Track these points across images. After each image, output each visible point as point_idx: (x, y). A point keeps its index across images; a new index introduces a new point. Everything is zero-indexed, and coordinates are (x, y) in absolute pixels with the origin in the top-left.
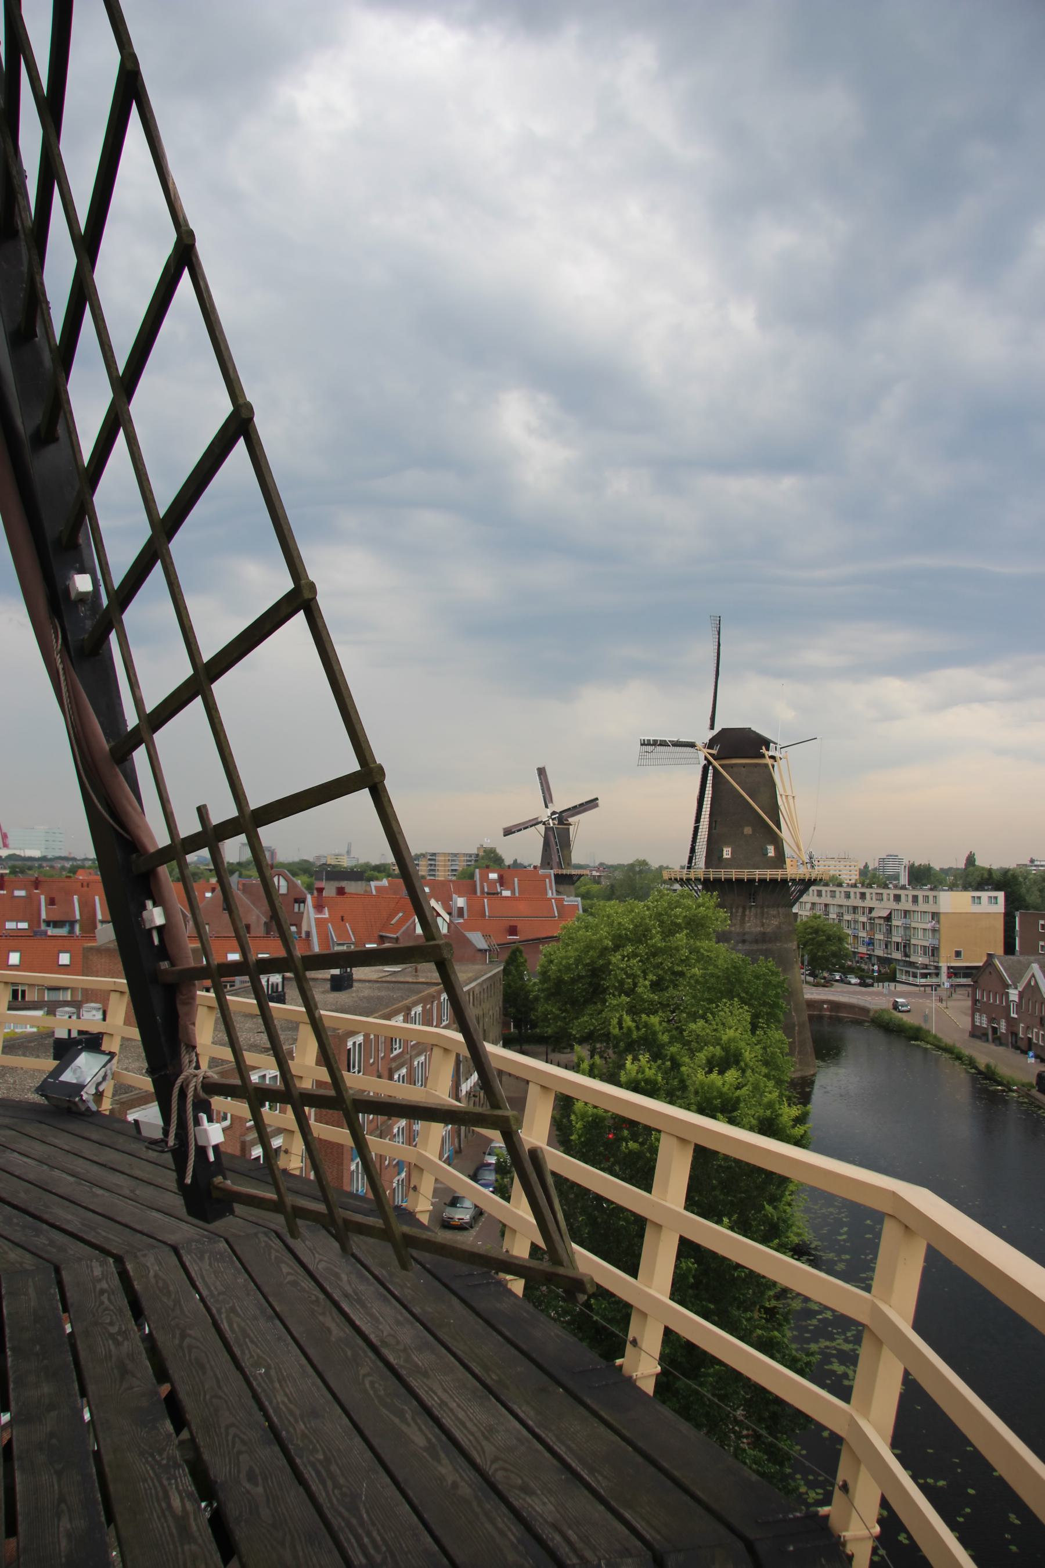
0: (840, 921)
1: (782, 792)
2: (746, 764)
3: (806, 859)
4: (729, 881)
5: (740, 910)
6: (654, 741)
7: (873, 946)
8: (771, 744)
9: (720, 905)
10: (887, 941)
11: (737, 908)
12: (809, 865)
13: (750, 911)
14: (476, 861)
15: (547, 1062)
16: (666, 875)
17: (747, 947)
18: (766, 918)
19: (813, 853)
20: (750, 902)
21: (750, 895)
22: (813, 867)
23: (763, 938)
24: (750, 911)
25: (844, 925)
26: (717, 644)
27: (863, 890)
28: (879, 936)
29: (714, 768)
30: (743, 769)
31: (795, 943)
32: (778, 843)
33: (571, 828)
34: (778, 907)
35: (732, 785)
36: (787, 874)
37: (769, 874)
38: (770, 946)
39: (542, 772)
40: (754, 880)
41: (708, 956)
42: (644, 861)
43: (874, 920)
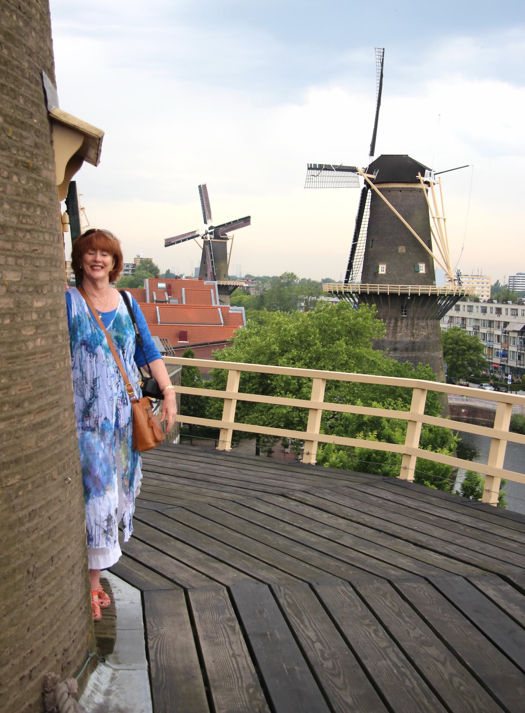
0: (476, 333)
1: (434, 215)
2: (402, 188)
3: (454, 276)
4: (384, 295)
5: (393, 321)
6: (320, 165)
7: (507, 357)
8: (426, 171)
9: (377, 317)
10: (521, 353)
11: (390, 319)
12: (456, 282)
13: (402, 323)
14: (133, 271)
15: (284, 438)
16: (326, 288)
17: (398, 354)
18: (416, 329)
19: (461, 271)
20: (402, 314)
21: (402, 308)
22: (460, 284)
23: (412, 347)
24: (402, 323)
25: (480, 337)
26: (380, 75)
27: (499, 306)
28: (512, 348)
29: (373, 191)
30: (399, 193)
31: (442, 352)
32: (428, 261)
33: (229, 243)
34: (427, 320)
35: (390, 208)
36: (436, 290)
37: (420, 289)
38: (418, 354)
39: (203, 190)
40: (406, 295)
41: (373, 361)
42: (292, 274)
43: (508, 333)
